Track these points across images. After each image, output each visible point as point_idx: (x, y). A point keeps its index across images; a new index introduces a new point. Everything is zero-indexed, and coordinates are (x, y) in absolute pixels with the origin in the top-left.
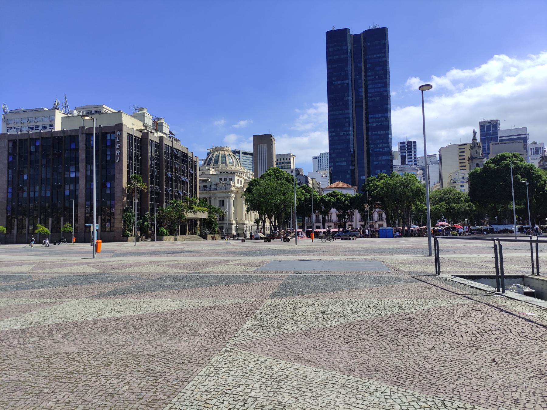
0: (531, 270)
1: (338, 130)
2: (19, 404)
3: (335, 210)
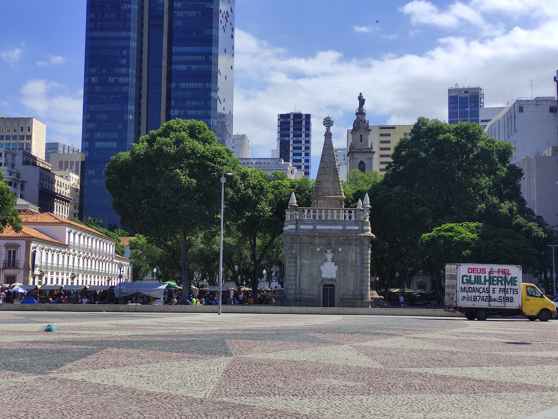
1: (104, 71)
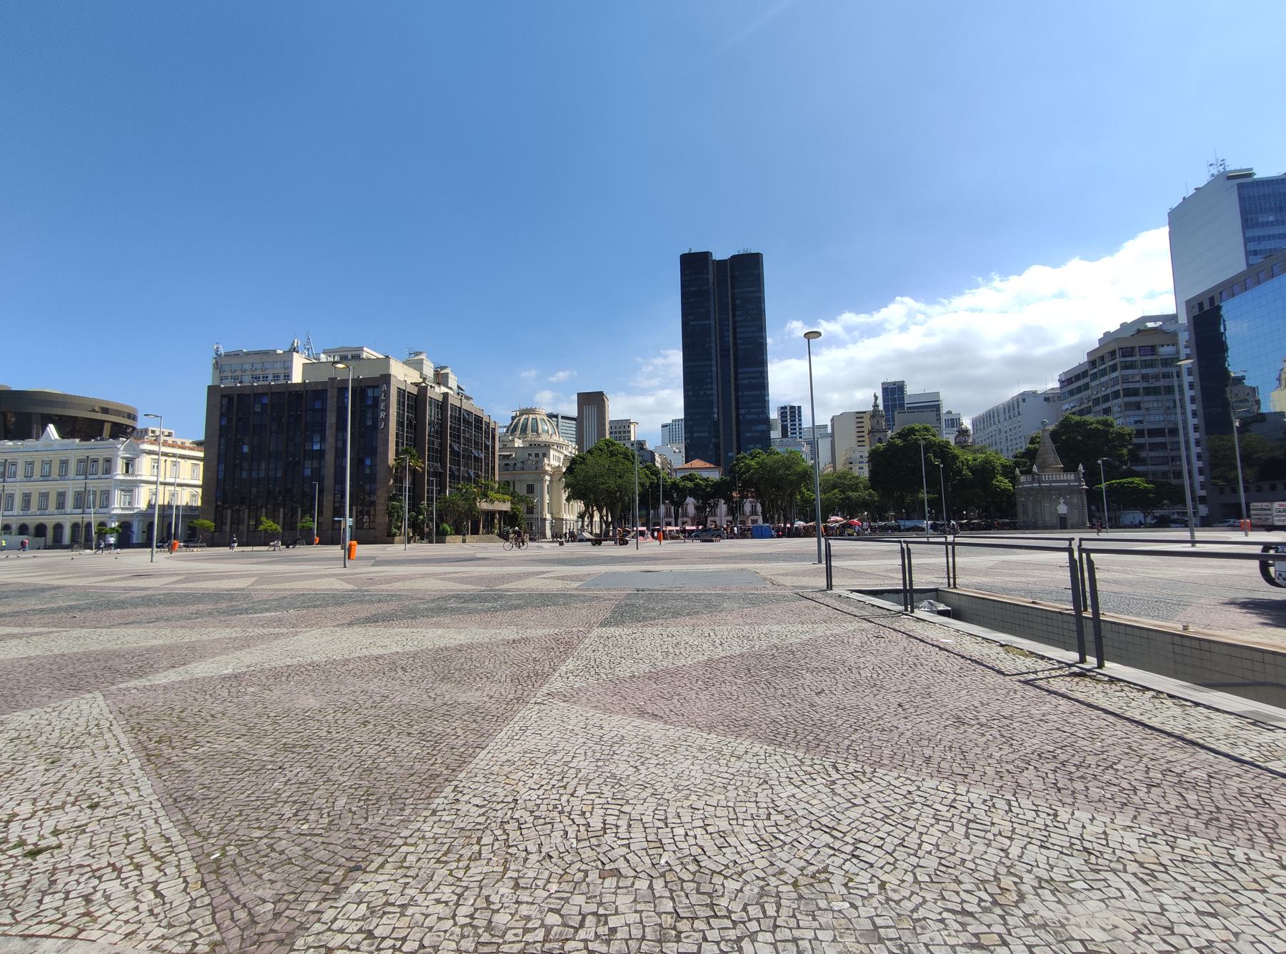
2: (228, 787)
3: (692, 499)
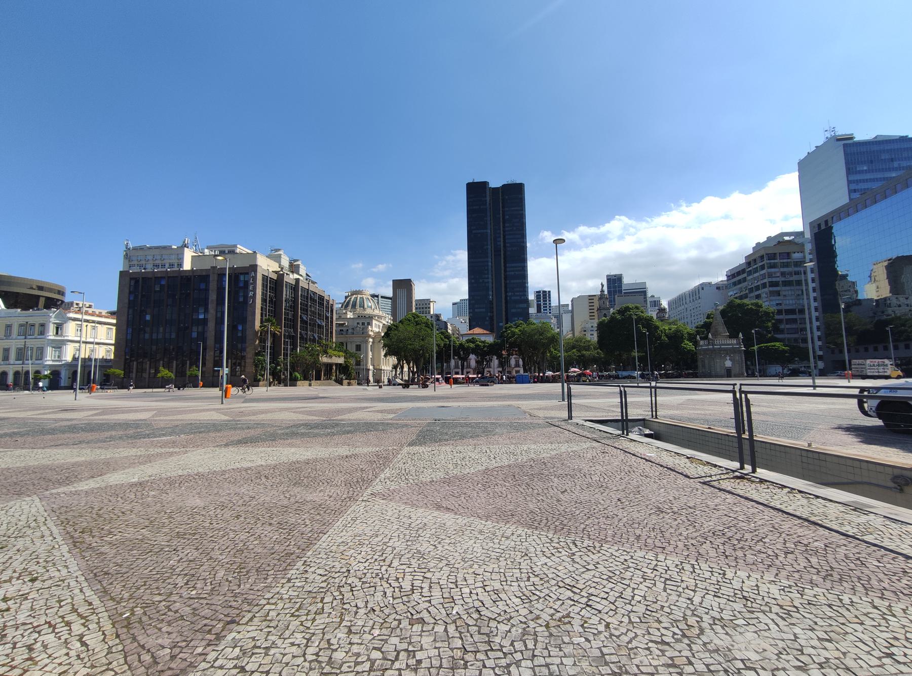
0: (650, 413)
3: (474, 356)
